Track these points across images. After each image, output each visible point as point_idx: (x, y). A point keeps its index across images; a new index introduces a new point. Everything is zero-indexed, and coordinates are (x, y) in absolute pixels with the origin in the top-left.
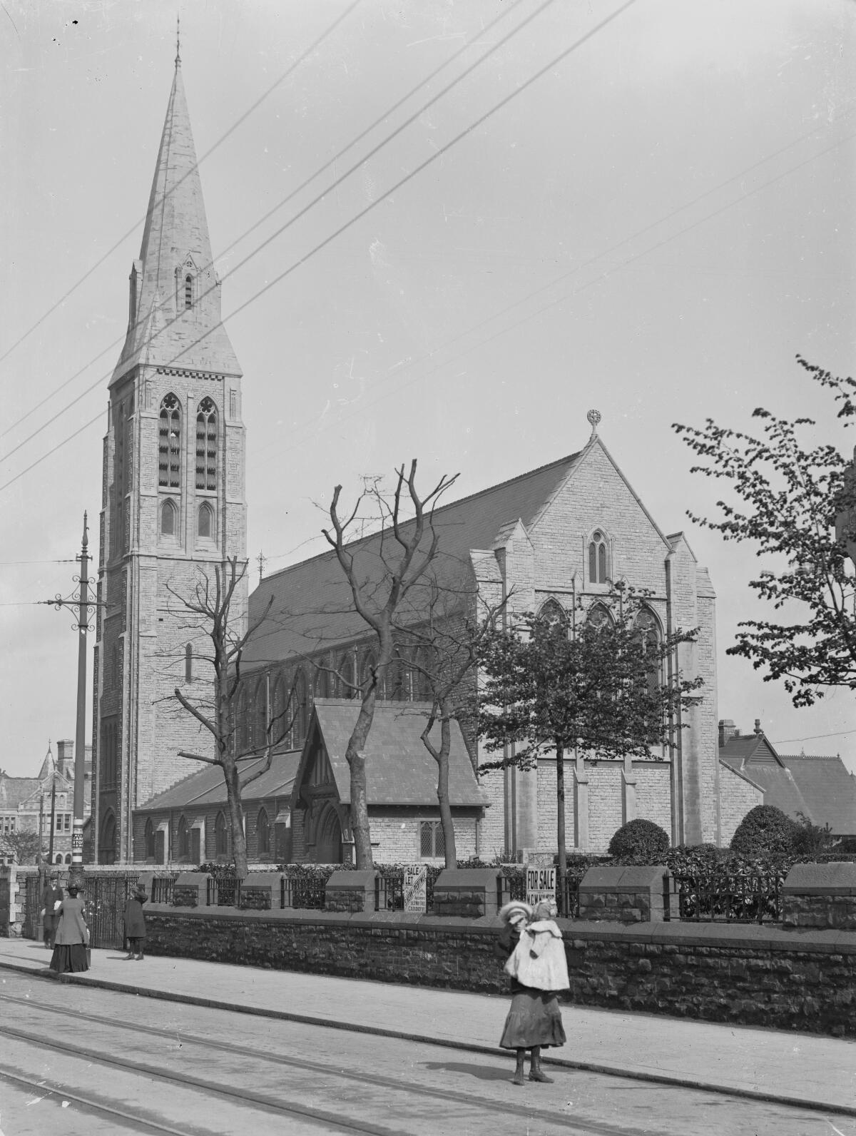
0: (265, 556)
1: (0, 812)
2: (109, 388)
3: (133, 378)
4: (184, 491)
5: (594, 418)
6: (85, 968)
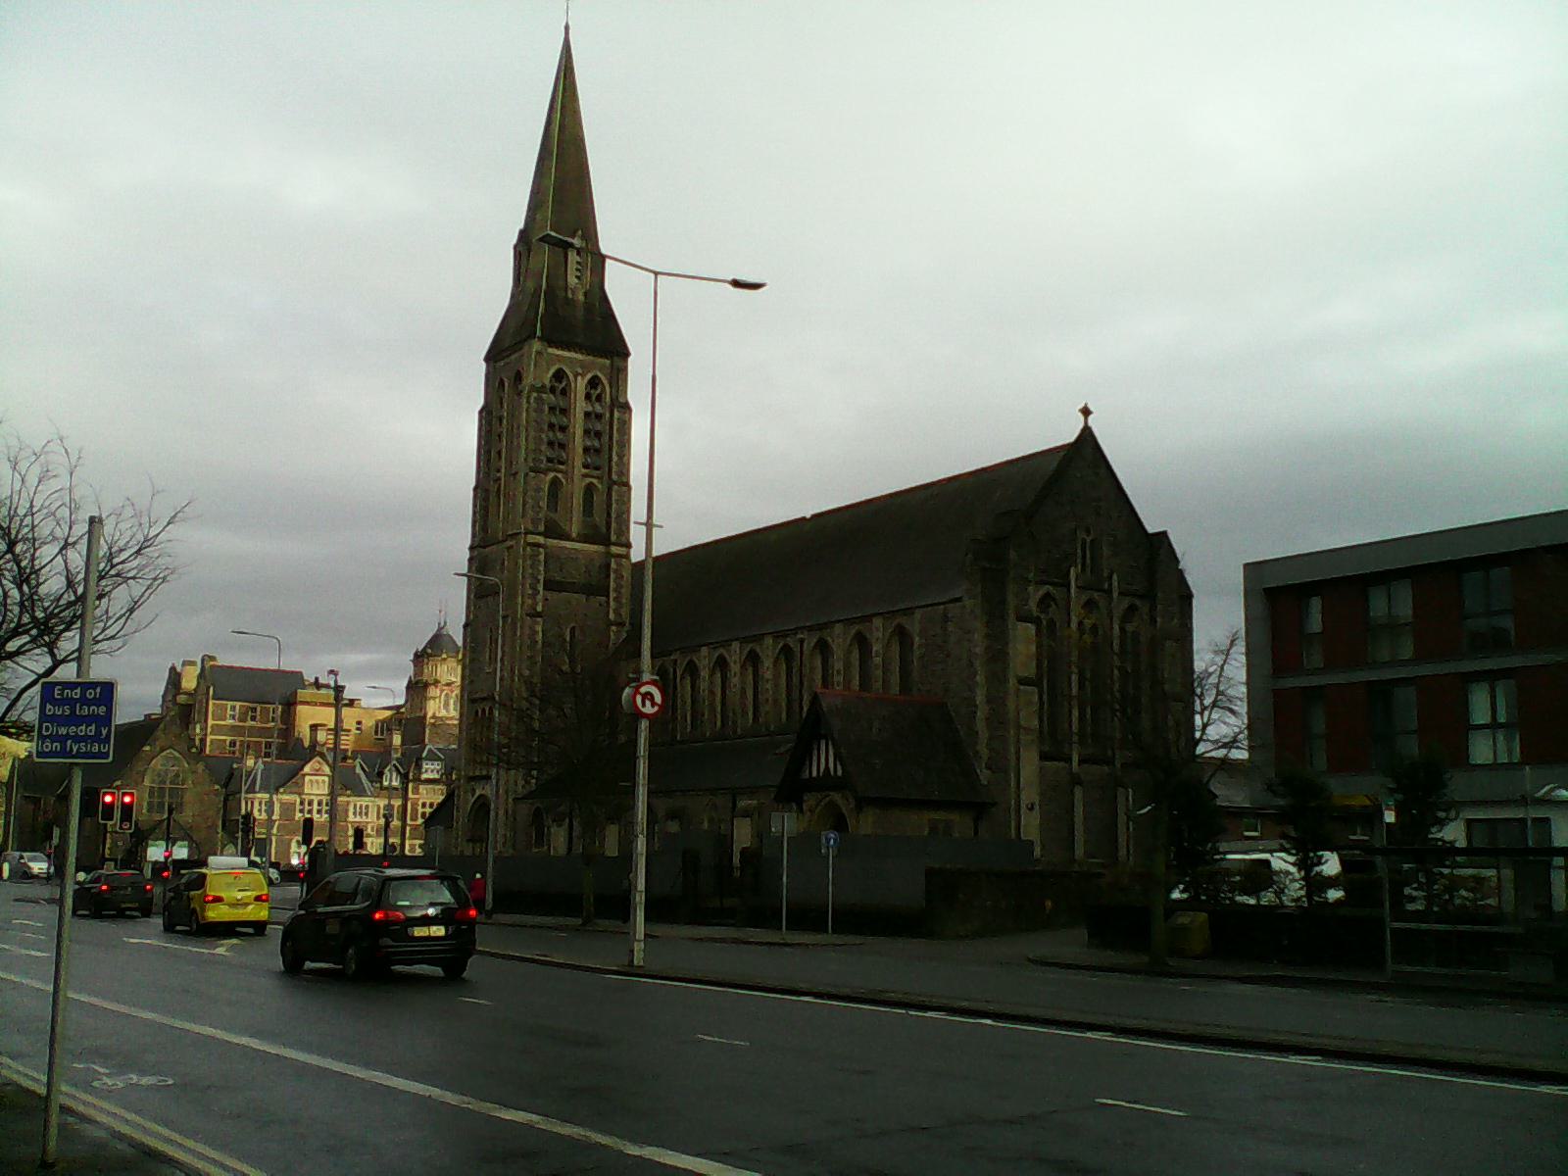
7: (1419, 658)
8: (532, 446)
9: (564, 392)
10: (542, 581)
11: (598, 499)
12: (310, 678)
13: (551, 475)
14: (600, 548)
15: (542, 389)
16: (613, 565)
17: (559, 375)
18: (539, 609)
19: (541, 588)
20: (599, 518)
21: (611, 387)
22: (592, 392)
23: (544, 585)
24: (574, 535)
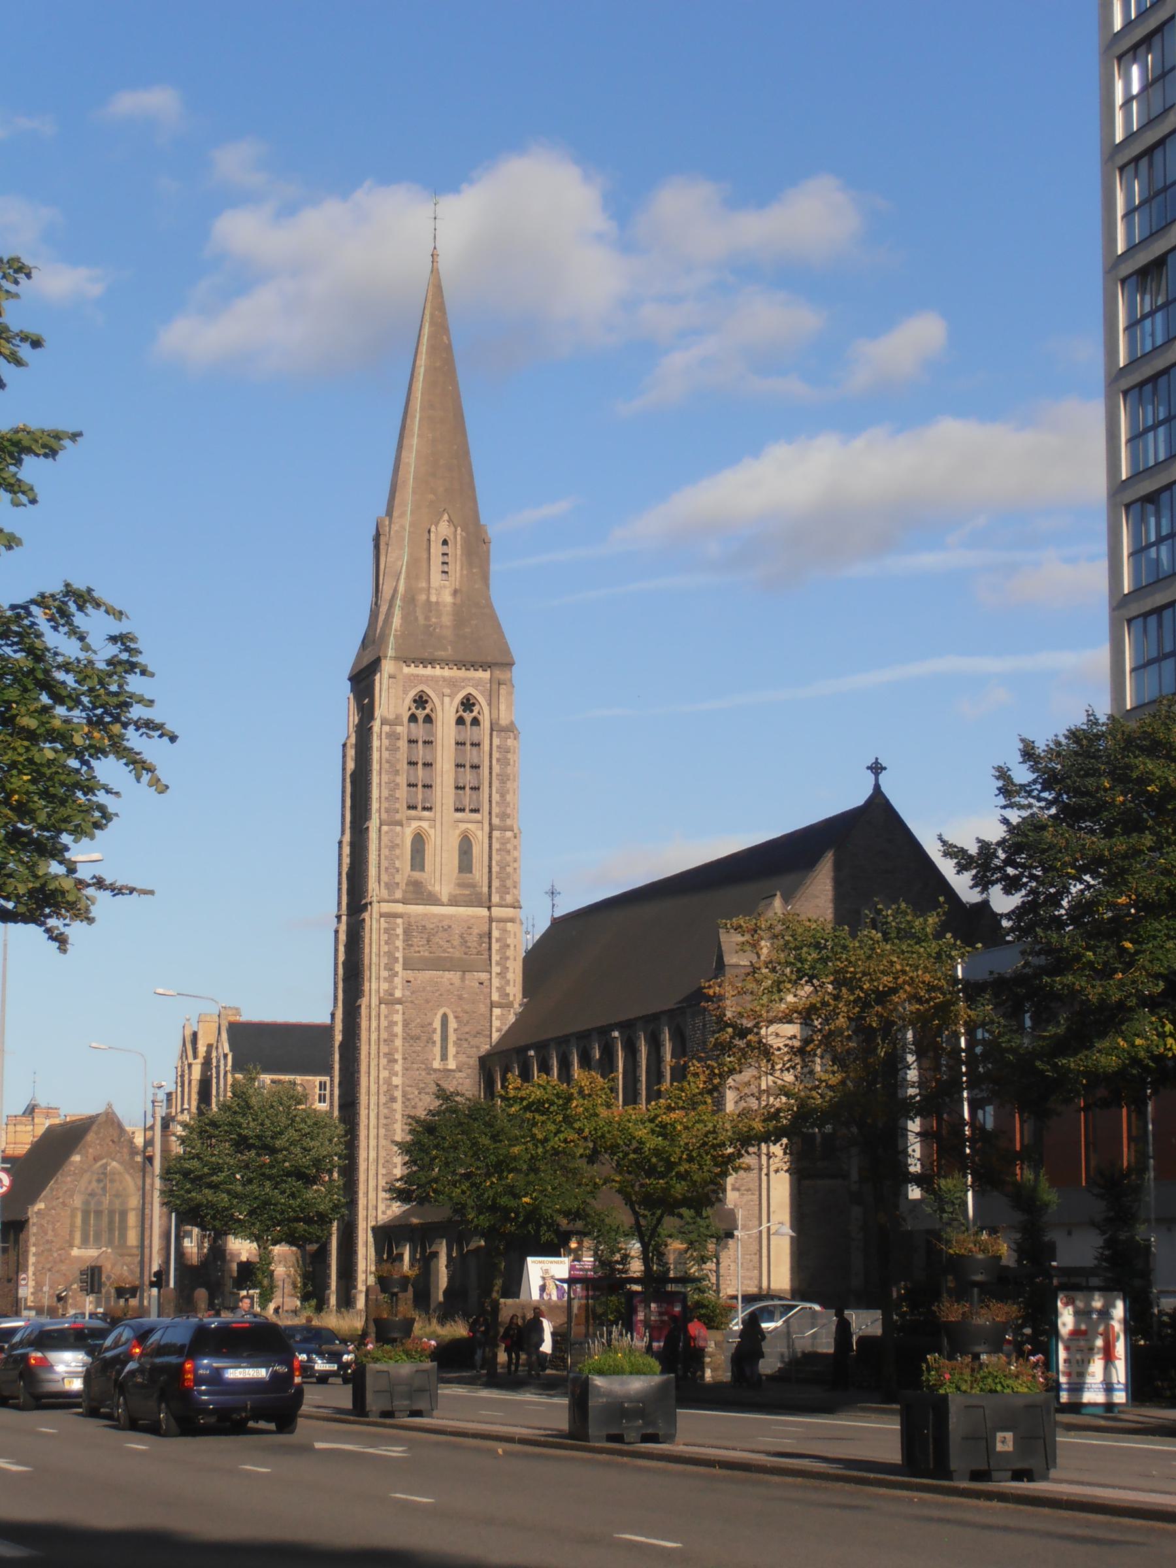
0: (558, 888)
1: (1175, 856)
2: (350, 679)
3: (374, 673)
4: (438, 815)
5: (877, 768)
6: (670, 1438)
7: (328, 1071)
8: (385, 793)
9: (428, 719)
10: (401, 960)
11: (479, 851)
12: (775, 1046)
13: (415, 824)
14: (484, 912)
15: (396, 722)
16: (495, 934)
17: (421, 701)
18: (398, 994)
19: (399, 967)
20: (479, 873)
21: (490, 705)
22: (465, 715)
23: (404, 964)
24: (445, 899)
